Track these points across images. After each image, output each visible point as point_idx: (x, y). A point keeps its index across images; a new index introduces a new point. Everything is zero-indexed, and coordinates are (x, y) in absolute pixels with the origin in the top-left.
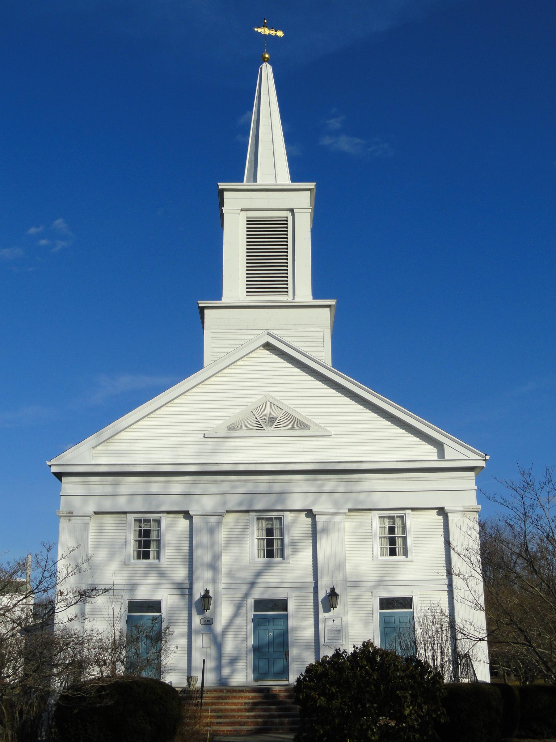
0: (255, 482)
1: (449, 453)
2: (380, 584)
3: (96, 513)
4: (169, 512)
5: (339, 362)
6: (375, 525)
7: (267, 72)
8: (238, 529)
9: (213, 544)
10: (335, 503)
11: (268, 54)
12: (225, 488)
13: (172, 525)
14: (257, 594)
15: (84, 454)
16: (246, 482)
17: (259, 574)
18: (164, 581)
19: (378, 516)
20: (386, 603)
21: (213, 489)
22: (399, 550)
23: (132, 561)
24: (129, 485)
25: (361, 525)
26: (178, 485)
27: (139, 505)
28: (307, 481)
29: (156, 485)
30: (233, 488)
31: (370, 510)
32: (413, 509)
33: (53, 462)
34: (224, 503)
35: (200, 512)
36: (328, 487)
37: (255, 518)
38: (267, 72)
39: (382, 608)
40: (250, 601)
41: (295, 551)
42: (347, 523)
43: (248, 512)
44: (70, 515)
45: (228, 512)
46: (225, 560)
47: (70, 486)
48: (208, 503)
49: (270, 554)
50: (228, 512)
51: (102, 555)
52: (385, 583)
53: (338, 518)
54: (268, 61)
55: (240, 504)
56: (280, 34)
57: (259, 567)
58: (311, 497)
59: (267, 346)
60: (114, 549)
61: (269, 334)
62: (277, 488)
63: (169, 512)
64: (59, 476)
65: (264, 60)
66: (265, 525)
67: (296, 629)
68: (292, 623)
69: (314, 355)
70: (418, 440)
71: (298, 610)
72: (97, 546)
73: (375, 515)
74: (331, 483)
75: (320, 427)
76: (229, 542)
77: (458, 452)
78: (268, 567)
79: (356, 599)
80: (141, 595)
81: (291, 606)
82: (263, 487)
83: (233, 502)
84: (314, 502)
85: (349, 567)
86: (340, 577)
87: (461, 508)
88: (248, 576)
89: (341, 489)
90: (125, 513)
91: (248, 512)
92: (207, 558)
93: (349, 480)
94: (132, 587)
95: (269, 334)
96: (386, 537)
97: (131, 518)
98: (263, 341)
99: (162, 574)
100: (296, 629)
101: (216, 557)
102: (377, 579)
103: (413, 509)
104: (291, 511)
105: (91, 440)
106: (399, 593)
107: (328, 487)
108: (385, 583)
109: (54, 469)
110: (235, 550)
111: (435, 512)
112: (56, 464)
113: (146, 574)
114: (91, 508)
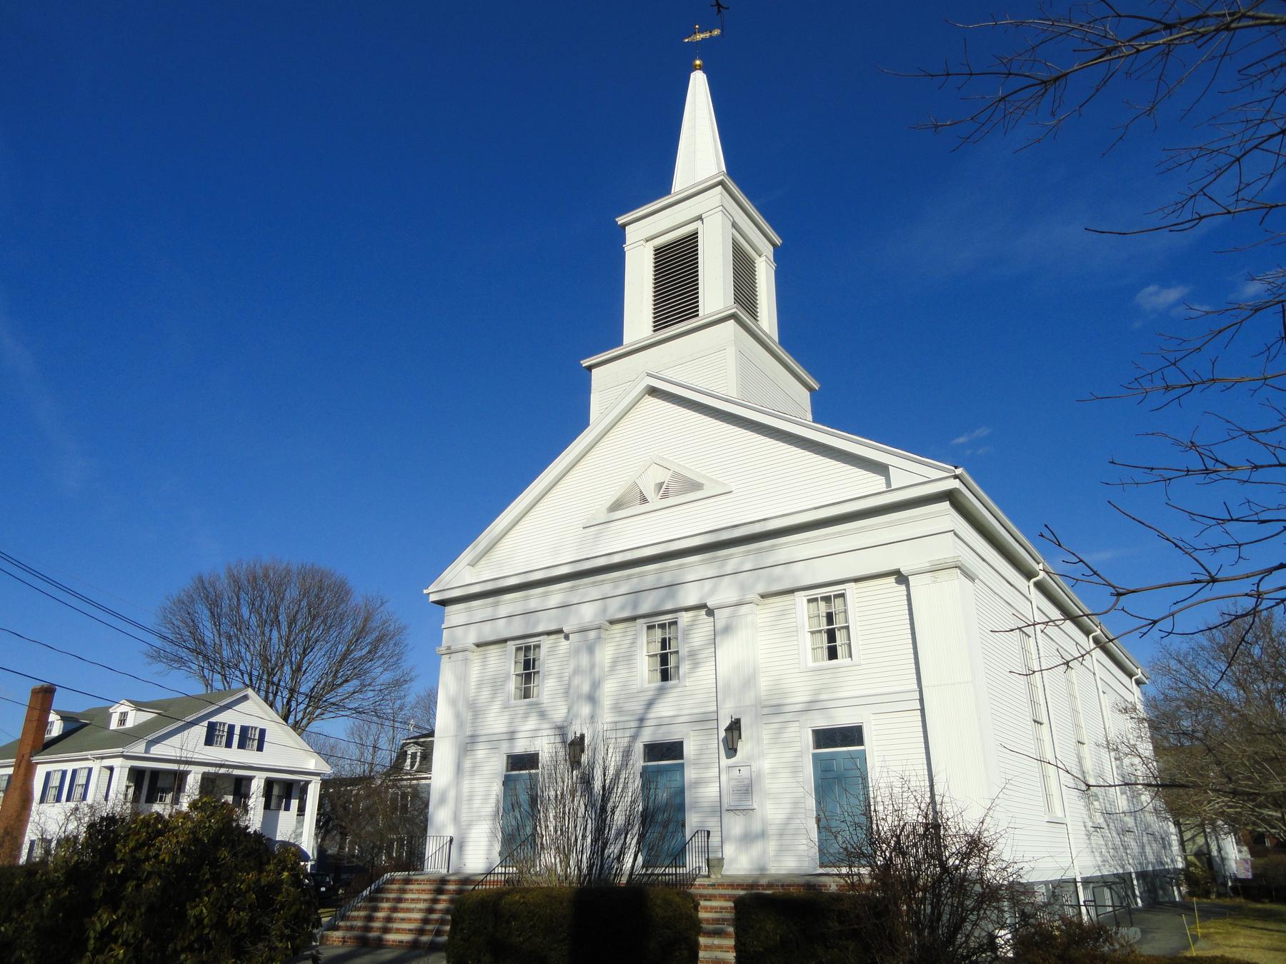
0: (641, 575)
1: (897, 478)
2: (811, 706)
3: (478, 645)
4: (549, 633)
5: (824, 412)
6: (801, 610)
7: (698, 85)
8: (627, 641)
9: (592, 667)
10: (742, 587)
11: (695, 59)
12: (607, 589)
13: (553, 649)
14: (647, 736)
15: (462, 574)
16: (629, 577)
17: (650, 704)
18: (546, 726)
19: (805, 600)
20: (825, 738)
21: (595, 593)
22: (840, 652)
23: (513, 702)
24: (509, 604)
25: (783, 613)
26: (556, 594)
27: (517, 628)
28: (703, 562)
29: (534, 598)
30: (616, 587)
31: (792, 591)
32: (856, 580)
33: (431, 589)
34: (604, 610)
35: (575, 628)
36: (730, 566)
37: (645, 627)
38: (698, 85)
39: (818, 744)
40: (639, 748)
41: (696, 665)
42: (760, 615)
43: (634, 619)
44: (450, 652)
45: (612, 622)
46: (609, 689)
47: (455, 615)
48: (588, 613)
49: (665, 676)
50: (612, 622)
51: (485, 694)
52: (818, 706)
53: (744, 609)
54: (701, 68)
55: (623, 608)
56: (716, 32)
57: (649, 695)
58: (708, 585)
59: (653, 392)
60: (497, 686)
61: (649, 375)
62: (667, 578)
63: (549, 633)
64: (443, 603)
65: (695, 68)
66: (658, 634)
67: (697, 783)
68: (690, 774)
69: (721, 391)
70: (849, 467)
71: (701, 752)
72: (480, 684)
73: (801, 598)
74: (736, 558)
75: (716, 482)
76: (615, 663)
77: (914, 473)
78: (661, 692)
79: (779, 733)
80: (521, 747)
81: (689, 749)
82: (649, 581)
83: (616, 609)
84: (713, 591)
85: (764, 684)
86: (749, 698)
87: (925, 565)
88: (637, 706)
89: (748, 566)
90: (505, 641)
91: (634, 619)
92: (586, 688)
93: (759, 551)
94: (511, 736)
95: (649, 375)
96: (820, 631)
97: (511, 646)
98: (642, 386)
99: (543, 715)
100: (697, 783)
101: (596, 685)
102: (808, 699)
103: (856, 580)
104: (687, 609)
105: (468, 555)
106: (843, 719)
107: (730, 566)
108: (818, 706)
109: (433, 598)
110: (622, 672)
111: (892, 579)
112: (433, 592)
113: (526, 716)
114: (472, 637)
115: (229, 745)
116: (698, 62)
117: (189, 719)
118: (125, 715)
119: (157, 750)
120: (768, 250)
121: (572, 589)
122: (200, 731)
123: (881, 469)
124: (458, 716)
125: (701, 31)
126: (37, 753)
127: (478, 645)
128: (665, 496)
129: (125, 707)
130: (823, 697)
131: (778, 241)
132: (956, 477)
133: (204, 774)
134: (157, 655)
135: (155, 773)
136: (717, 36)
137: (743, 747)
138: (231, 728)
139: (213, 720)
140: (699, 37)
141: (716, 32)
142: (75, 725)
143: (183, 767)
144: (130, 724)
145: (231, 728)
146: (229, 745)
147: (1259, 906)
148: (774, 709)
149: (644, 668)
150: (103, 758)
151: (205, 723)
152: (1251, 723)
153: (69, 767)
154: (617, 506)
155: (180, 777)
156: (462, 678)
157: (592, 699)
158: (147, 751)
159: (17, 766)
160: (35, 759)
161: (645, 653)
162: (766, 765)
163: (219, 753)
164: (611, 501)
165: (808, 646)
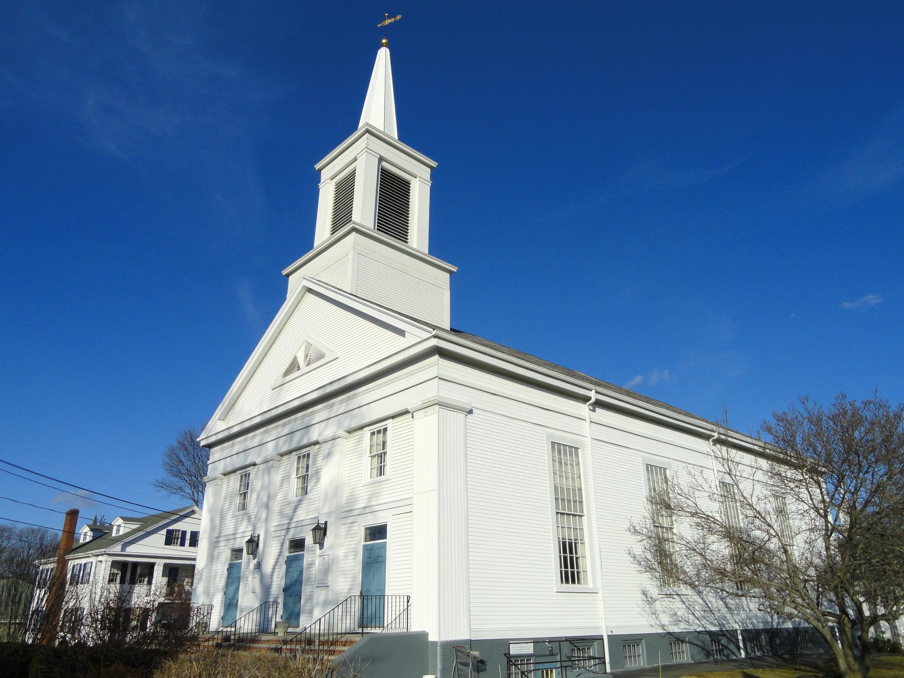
7: (383, 57)
14: (290, 536)
15: (217, 426)
32: (393, 417)
33: (201, 437)
38: (383, 57)
42: (346, 444)
45: (282, 455)
50: (282, 455)
54: (387, 45)
56: (398, 17)
64: (210, 446)
65: (382, 45)
93: (349, 399)
103: (393, 417)
108: (368, 510)
109: (203, 443)
115: (182, 544)
116: (384, 41)
117: (149, 529)
118: (120, 527)
119: (130, 549)
120: (426, 173)
121: (266, 432)
122: (161, 536)
123: (402, 333)
124: (212, 521)
125: (389, 18)
126: (69, 553)
127: (225, 475)
128: (308, 364)
129: (120, 521)
130: (373, 503)
131: (434, 164)
132: (435, 337)
133: (165, 565)
134: (162, 485)
135: (135, 565)
136: (400, 20)
137: (327, 542)
138: (184, 533)
139: (171, 528)
140: (387, 22)
141: (398, 17)
142: (101, 534)
143: (152, 560)
144: (121, 533)
145: (184, 533)
146: (182, 544)
147: (439, 651)
148: (347, 513)
149: (294, 483)
150: (98, 555)
151: (164, 532)
152: (871, 492)
153: (83, 561)
154: (288, 372)
155: (152, 566)
156: (216, 495)
157: (267, 507)
158: (123, 549)
159: (58, 562)
160: (67, 557)
161: (295, 476)
162: (341, 552)
163: (175, 551)
164: (284, 368)
165: (367, 463)
